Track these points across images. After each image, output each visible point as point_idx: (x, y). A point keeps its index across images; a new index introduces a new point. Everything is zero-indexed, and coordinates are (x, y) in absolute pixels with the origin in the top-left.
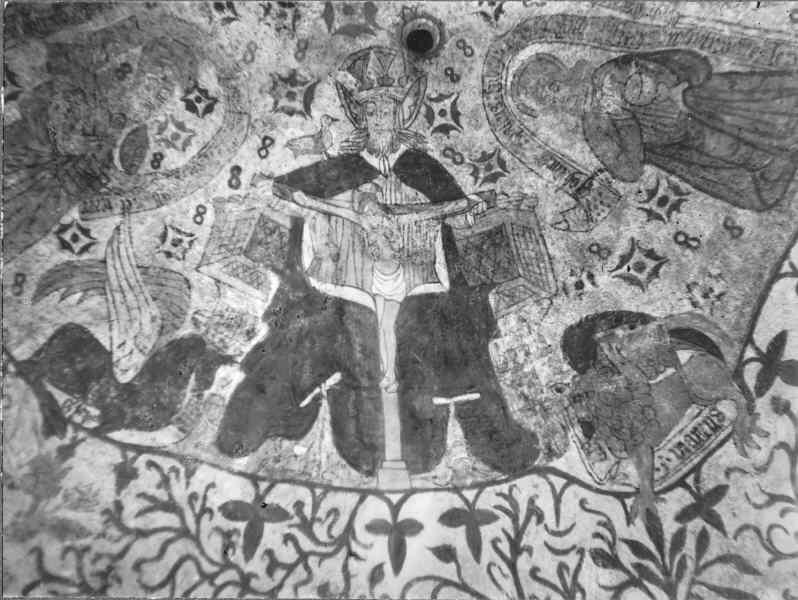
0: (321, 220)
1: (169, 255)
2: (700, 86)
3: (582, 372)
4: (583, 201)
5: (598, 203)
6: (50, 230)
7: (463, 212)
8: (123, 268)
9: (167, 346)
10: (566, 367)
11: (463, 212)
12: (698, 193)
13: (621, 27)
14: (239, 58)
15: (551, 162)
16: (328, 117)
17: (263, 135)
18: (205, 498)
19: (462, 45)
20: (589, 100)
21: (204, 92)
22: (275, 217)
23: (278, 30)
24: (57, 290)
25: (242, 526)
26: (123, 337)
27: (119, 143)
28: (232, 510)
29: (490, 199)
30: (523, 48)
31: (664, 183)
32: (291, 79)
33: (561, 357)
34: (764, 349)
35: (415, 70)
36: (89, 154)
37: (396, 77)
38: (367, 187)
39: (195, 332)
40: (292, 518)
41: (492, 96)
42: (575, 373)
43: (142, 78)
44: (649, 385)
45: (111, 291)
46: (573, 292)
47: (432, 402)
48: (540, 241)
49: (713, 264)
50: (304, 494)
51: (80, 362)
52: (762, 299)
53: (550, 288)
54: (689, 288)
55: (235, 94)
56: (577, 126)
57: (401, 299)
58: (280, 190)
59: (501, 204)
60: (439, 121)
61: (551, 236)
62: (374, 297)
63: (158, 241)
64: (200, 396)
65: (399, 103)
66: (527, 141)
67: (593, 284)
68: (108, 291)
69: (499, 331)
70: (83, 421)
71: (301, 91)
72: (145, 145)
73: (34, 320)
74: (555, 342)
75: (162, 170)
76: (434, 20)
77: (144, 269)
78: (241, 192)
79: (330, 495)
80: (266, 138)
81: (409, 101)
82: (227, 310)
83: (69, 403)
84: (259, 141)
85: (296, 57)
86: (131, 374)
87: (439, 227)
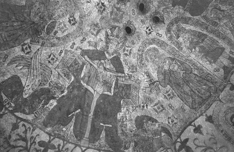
0: (89, 66)
1: (49, 62)
2: (188, 74)
3: (138, 129)
4: (151, 87)
5: (154, 89)
6: (21, 44)
7: (123, 77)
8: (36, 62)
9: (40, 89)
10: (134, 126)
11: (123, 77)
12: (178, 97)
13: (175, 51)
14: (87, 13)
15: (148, 74)
16: (101, 39)
17: (84, 37)
18: (35, 138)
19: (138, 36)
20: (162, 64)
21: (75, 19)
22: (79, 60)
23: (99, 11)
24: (16, 63)
25: (42, 149)
26: (29, 84)
27: (48, 24)
28: (41, 144)
29: (130, 77)
30: (152, 44)
31: (171, 91)
32: (96, 25)
33: (134, 123)
34: (182, 141)
35: (125, 37)
36: (39, 24)
37: (120, 37)
38: (103, 61)
39: (49, 87)
40: (56, 149)
41: (140, 52)
42: (136, 128)
43: (60, 7)
44: (153, 138)
45: (31, 68)
46: (141, 108)
47: (100, 124)
48: (138, 92)
49: (176, 115)
50: (61, 142)
51: (14, 88)
52: (185, 128)
53: (136, 105)
54: (169, 118)
55: (81, 23)
56: (157, 69)
57: (101, 94)
58: (82, 53)
59: (132, 79)
60: (126, 52)
61: (141, 91)
62: (95, 91)
63: (48, 57)
64: (43, 107)
65: (119, 43)
66: (144, 67)
67: (147, 108)
68: (30, 68)
69: (121, 111)
70: (9, 107)
71: (97, 30)
72: (54, 27)
73: (6, 71)
74: (133, 118)
75: (56, 36)
76: (134, 27)
77: (41, 64)
78: (73, 50)
79: (68, 144)
80: (84, 38)
81: (121, 44)
82: (59, 83)
83: (6, 100)
84: (82, 38)
85: (100, 19)
86: (27, 95)
87: (116, 78)
